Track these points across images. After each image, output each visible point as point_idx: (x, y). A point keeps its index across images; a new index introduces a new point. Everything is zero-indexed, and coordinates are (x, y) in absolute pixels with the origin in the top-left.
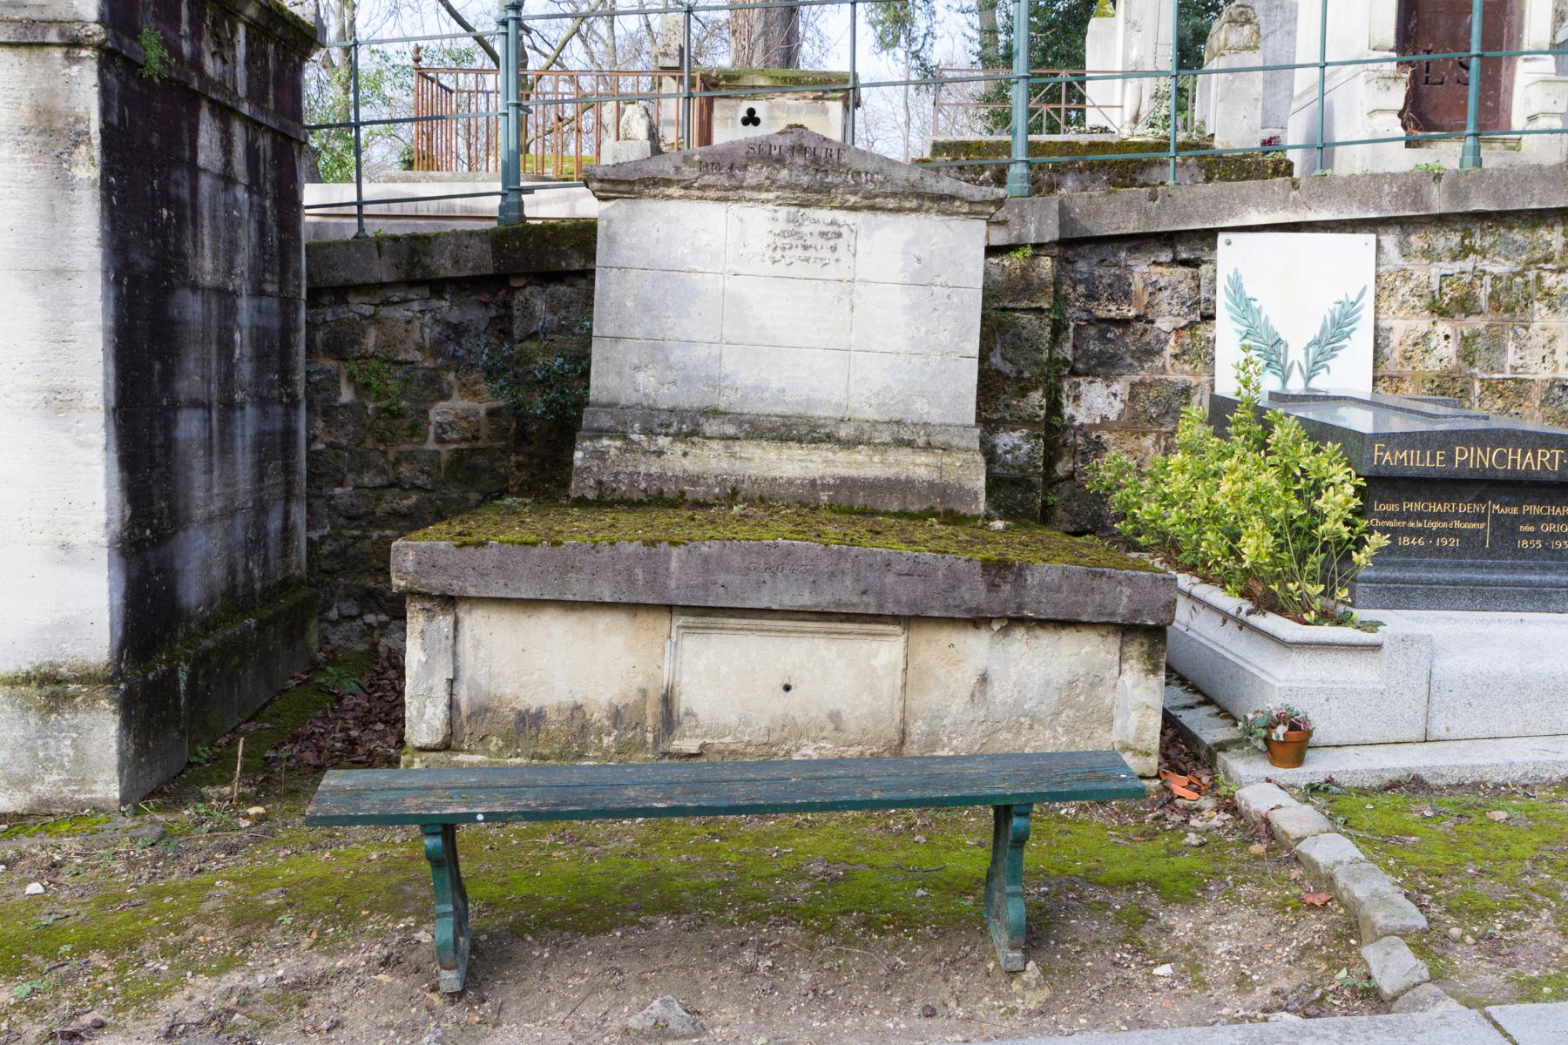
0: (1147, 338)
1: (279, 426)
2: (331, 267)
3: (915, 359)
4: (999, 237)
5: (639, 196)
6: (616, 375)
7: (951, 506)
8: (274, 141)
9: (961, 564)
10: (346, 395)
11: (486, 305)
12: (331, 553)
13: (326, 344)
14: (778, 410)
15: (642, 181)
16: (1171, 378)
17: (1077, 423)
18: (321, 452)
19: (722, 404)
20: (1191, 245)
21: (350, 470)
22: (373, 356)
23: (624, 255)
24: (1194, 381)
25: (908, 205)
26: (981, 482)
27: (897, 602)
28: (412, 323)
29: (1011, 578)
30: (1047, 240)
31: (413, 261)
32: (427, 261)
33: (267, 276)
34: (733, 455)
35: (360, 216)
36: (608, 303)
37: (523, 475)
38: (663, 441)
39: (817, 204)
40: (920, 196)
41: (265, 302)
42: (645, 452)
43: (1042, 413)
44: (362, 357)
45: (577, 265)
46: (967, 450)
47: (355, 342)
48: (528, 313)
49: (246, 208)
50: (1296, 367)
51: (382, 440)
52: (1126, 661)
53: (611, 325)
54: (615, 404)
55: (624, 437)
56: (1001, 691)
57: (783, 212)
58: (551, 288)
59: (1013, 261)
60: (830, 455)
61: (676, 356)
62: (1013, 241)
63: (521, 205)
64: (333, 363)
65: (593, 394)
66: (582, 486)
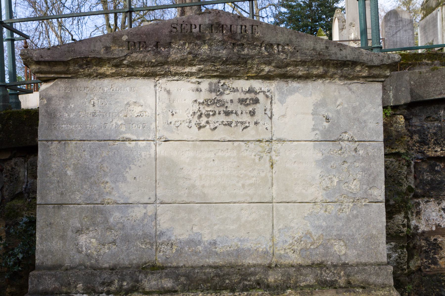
3: (331, 207)
5: (75, 76)
14: (211, 261)
15: (75, 61)
17: (420, 231)
25: (315, 72)
30: (402, 102)
36: (50, 174)
39: (236, 75)
40: (325, 63)
46: (384, 286)
53: (53, 193)
54: (60, 266)
57: (205, 84)
61: (115, 217)
65: (39, 258)
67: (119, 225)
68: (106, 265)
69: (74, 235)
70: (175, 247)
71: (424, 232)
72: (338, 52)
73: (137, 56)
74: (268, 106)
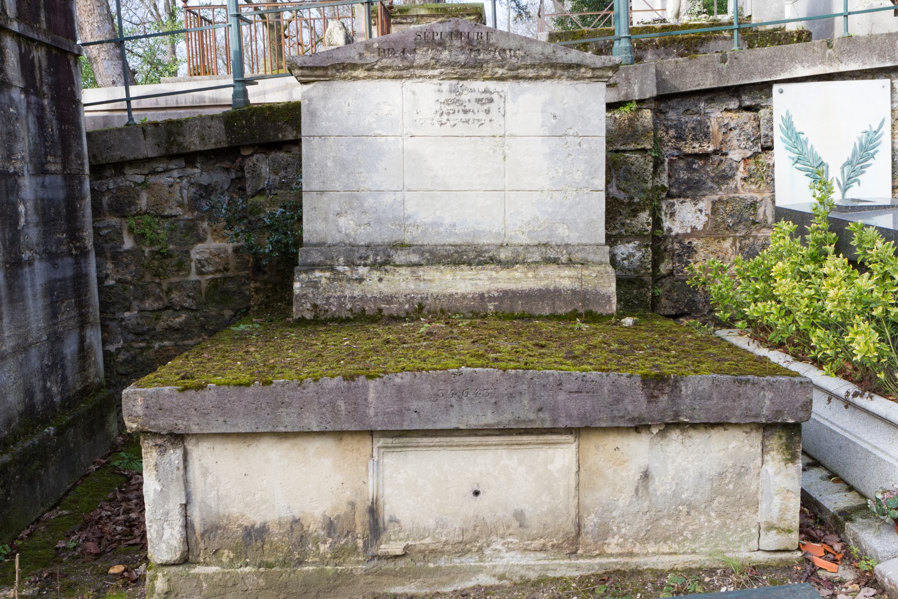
0: (722, 167)
1: (69, 273)
2: (109, 148)
3: (556, 194)
4: (613, 97)
5: (333, 78)
6: (322, 222)
7: (591, 308)
8: (48, 53)
9: (624, 380)
10: (128, 243)
11: (227, 170)
12: (125, 361)
13: (110, 206)
14: (451, 241)
15: (333, 66)
16: (742, 196)
17: (673, 233)
18: (112, 287)
19: (407, 238)
20: (752, 95)
21: (135, 298)
22: (146, 213)
23: (323, 126)
24: (759, 197)
25: (544, 74)
26: (613, 288)
27: (569, 416)
28: (174, 186)
29: (667, 389)
30: (648, 96)
31: (170, 140)
32: (180, 139)
33: (50, 158)
34: (418, 278)
35: (129, 110)
36: (313, 165)
37: (260, 298)
38: (362, 271)
39: (473, 77)
40: (553, 66)
41: (48, 179)
42: (349, 280)
43: (649, 228)
44: (138, 214)
45: (290, 137)
46: (600, 263)
47: (132, 203)
48: (257, 176)
49: (23, 107)
50: (835, 180)
51: (157, 275)
52: (768, 452)
53: (316, 182)
54: (324, 244)
55: (332, 269)
56: (661, 485)
57: (446, 85)
58: (273, 155)
59: (622, 114)
60: (494, 274)
61: (369, 202)
62: (622, 99)
63: (245, 92)
64: (116, 220)
65: (306, 237)
66: (302, 309)
67: (373, 210)
68: (363, 243)
69: (335, 218)
70: (420, 229)
71: (677, 235)
72: (564, 56)
73: (386, 62)
74: (502, 105)
